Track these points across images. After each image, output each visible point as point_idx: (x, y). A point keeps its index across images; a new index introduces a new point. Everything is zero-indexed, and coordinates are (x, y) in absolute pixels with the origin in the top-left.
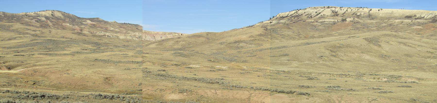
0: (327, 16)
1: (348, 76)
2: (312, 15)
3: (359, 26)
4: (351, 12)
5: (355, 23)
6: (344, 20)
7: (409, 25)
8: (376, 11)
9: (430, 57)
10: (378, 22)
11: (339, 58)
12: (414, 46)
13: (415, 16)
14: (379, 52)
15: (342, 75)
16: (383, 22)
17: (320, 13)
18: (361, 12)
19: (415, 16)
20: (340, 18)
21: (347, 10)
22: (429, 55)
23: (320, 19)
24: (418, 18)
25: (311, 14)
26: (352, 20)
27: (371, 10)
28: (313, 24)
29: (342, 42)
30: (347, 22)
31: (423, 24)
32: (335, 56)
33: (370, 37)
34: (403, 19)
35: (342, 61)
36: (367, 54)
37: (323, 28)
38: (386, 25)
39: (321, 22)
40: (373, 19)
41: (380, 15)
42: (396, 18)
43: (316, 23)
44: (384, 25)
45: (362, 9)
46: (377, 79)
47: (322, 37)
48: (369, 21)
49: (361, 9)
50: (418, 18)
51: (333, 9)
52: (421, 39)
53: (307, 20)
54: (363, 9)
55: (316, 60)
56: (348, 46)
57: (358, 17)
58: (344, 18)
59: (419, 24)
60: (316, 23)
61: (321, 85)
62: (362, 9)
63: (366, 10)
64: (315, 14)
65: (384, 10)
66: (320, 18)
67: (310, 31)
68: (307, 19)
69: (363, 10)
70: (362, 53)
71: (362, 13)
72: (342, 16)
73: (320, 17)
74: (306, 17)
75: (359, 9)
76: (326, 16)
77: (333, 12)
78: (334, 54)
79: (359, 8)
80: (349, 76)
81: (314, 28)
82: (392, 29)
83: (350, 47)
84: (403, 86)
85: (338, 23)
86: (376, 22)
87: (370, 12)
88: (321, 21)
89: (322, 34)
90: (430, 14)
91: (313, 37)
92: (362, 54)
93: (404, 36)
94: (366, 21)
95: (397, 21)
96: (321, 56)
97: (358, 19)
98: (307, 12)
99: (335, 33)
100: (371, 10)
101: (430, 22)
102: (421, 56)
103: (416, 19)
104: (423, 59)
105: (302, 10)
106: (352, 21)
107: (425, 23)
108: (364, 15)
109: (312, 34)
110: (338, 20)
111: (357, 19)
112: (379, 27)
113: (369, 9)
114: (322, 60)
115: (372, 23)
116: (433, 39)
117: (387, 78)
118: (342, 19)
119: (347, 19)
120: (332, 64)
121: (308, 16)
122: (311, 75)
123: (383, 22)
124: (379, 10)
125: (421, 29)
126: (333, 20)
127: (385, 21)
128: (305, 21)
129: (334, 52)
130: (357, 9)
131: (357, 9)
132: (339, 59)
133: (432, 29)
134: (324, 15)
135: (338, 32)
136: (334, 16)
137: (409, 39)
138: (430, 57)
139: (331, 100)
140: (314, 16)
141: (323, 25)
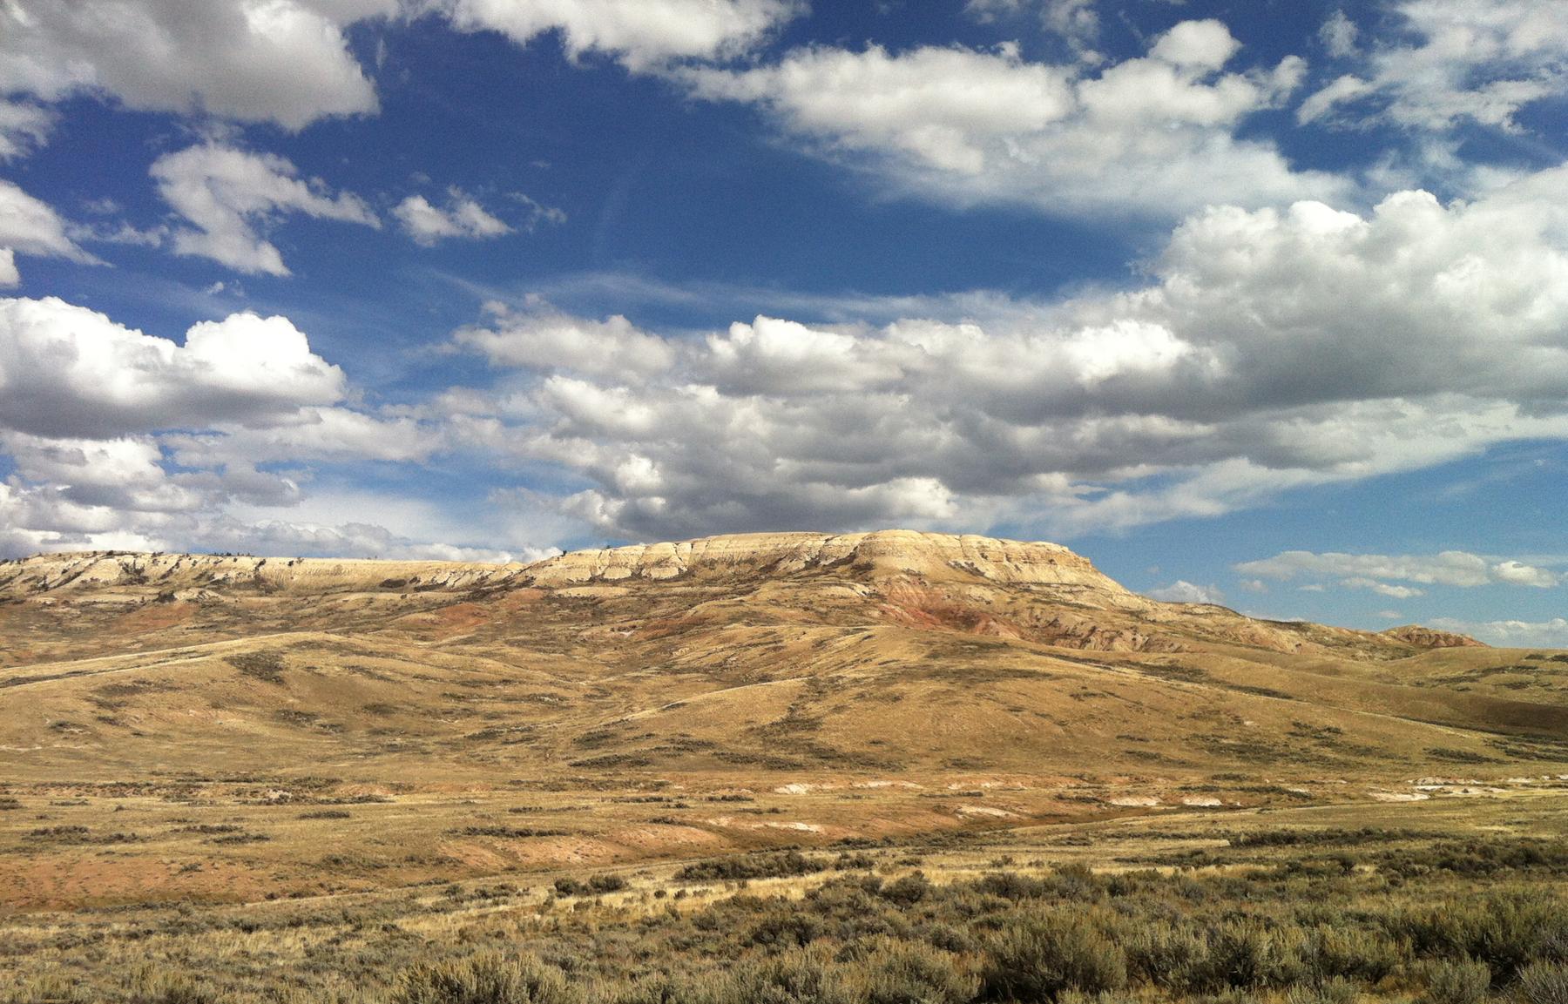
0: (106, 583)
1: (144, 790)
2: (48, 581)
3: (217, 617)
4: (191, 570)
5: (204, 606)
6: (165, 596)
7: (396, 610)
8: (283, 567)
9: (451, 713)
10: (287, 602)
11: (125, 726)
12: (399, 678)
13: (415, 580)
14: (277, 702)
15: (123, 788)
16: (306, 602)
17: (78, 574)
18: (229, 568)
19: (415, 580)
20: (150, 592)
21: (177, 564)
22: (450, 704)
23: (79, 595)
24: (424, 588)
25: (45, 578)
26: (195, 596)
27: (262, 563)
28: (51, 610)
29: (142, 672)
30: (176, 605)
31: (440, 605)
32: (111, 722)
33: (248, 651)
34: (373, 590)
35: (139, 739)
36: (230, 710)
37: (89, 625)
38: (315, 610)
39: (82, 605)
40: (269, 592)
41: (296, 578)
42: (351, 588)
43: (60, 610)
44: (308, 611)
45: (233, 558)
46: (248, 794)
47: (76, 655)
48: (255, 599)
49: (228, 561)
50: (424, 588)
51: (129, 560)
52: (426, 655)
53: (29, 599)
54: (235, 560)
55: (37, 740)
56: (165, 686)
57: (219, 585)
58: (166, 590)
59: (428, 607)
60: (61, 610)
61: (20, 829)
62: (233, 558)
63: (247, 563)
64: (62, 579)
65: (307, 561)
66: (79, 591)
67: (37, 638)
68: (28, 596)
69: (234, 564)
70: (216, 706)
71: (233, 574)
72: (161, 582)
73: (77, 588)
74: (27, 586)
75: (220, 559)
76: (100, 585)
77: (127, 571)
78: (110, 714)
79: (222, 555)
80: (147, 788)
81: (55, 625)
82: (336, 623)
83: (171, 689)
84: (317, 816)
85: (145, 608)
86: (281, 603)
87: (261, 568)
88: (81, 600)
89: (83, 646)
90: (466, 572)
91: (45, 658)
92: (213, 712)
93: (371, 647)
94: (244, 599)
95: (353, 597)
96: (61, 725)
97: (216, 595)
98: (31, 570)
99: (129, 641)
100: (262, 563)
101: (463, 599)
102: (421, 711)
103: (417, 590)
104: (430, 719)
105: (12, 562)
106: (196, 601)
107: (449, 604)
108: (239, 581)
109: (40, 647)
110: (146, 599)
111: (212, 594)
112: (288, 619)
113: (258, 560)
114: (62, 736)
115: (265, 607)
116: (471, 655)
117: (1410, 764)
118: (159, 594)
119: (176, 596)
120: (97, 750)
121: (32, 583)
122: (7, 793)
123: (306, 602)
124: (291, 564)
125: (432, 622)
126: (125, 599)
127: (310, 599)
128: (22, 602)
129: (110, 706)
130: (213, 560)
131: (213, 560)
132: (126, 732)
133: (472, 620)
134: (92, 579)
135: (141, 637)
136: (130, 582)
137: (386, 655)
138: (451, 713)
139: (28, 881)
140: (56, 584)
141: (89, 616)
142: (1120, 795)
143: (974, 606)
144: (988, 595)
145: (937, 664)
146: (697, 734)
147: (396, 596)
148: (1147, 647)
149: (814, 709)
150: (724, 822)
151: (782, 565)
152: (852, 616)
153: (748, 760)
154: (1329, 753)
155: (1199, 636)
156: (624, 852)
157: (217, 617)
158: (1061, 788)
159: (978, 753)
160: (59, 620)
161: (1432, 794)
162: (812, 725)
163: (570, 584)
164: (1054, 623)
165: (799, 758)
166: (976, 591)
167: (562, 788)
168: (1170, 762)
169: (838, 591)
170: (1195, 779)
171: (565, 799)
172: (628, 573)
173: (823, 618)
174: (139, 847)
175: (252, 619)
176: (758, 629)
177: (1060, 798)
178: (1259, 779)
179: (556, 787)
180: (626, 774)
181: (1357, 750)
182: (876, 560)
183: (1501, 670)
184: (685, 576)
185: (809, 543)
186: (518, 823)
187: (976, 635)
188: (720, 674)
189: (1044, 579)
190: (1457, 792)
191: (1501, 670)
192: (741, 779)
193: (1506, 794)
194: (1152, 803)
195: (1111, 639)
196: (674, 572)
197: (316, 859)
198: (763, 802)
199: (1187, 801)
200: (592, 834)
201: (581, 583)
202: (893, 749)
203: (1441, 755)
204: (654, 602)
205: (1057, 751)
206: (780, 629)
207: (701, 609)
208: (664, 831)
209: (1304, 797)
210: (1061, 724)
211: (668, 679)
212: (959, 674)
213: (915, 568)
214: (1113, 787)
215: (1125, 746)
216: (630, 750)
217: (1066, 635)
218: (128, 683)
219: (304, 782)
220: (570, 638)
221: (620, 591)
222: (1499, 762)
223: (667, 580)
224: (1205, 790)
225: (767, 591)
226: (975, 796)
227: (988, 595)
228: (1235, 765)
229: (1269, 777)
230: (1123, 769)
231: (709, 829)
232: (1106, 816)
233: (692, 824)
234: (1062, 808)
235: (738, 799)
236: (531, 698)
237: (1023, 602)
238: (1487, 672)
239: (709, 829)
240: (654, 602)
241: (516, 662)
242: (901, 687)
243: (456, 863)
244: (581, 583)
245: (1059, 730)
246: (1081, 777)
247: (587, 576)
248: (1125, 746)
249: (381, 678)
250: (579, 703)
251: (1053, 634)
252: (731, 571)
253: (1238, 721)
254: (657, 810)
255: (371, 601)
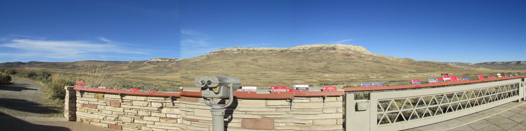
7: (271, 54)
13: (273, 50)
19: (273, 50)
20: (241, 52)
22: (279, 65)
32: (238, 66)
40: (255, 52)
42: (265, 51)
47: (233, 59)
49: (250, 48)
51: (238, 48)
56: (244, 62)
57: (249, 51)
58: (243, 52)
60: (230, 54)
63: (252, 48)
78: (238, 65)
81: (229, 55)
88: (232, 53)
91: (229, 59)
95: (265, 52)
115: (255, 53)
129: (238, 65)
133: (281, 55)
142: (371, 76)
143: (350, 54)
144: (352, 52)
145: (345, 61)
146: (313, 68)
147: (271, 52)
148: (373, 59)
149: (329, 66)
150: (319, 79)
151: (323, 48)
152: (333, 55)
153: (320, 72)
154: (397, 72)
155: (380, 58)
156: (306, 82)
157: (249, 54)
158: (363, 76)
159: (351, 71)
160: (230, 55)
161: (409, 76)
162: (328, 68)
163: (296, 50)
164: (360, 56)
165: (327, 72)
166: (350, 52)
167: (295, 74)
168: (377, 73)
169: (331, 51)
170: (380, 75)
171: (296, 76)
172: (302, 49)
173: (329, 55)
174: (246, 80)
175: (253, 55)
176: (320, 56)
177: (363, 77)
178: (388, 75)
179: (295, 74)
180: (303, 73)
181: (400, 71)
182: (336, 48)
183: (417, 63)
184: (309, 49)
185: (327, 45)
186: (292, 79)
187: (350, 57)
188: (315, 61)
189: (359, 51)
190: (412, 76)
191: (417, 63)
192: (319, 74)
193: (418, 76)
194: (375, 77)
195: (368, 58)
196: (308, 49)
197: (268, 82)
198: (323, 77)
199: (380, 77)
200: (301, 80)
201: (297, 50)
202: (340, 71)
203: (410, 72)
204: (305, 52)
205: (362, 72)
206: (323, 56)
207: (312, 53)
208: (311, 80)
209: (394, 77)
210: (362, 68)
211: (308, 62)
212: (348, 62)
213: (341, 49)
214: (370, 75)
215: (371, 71)
216: (303, 70)
217: (362, 57)
218: (240, 62)
219: (263, 74)
220: (296, 57)
221: (302, 51)
222: (417, 73)
223: (307, 50)
224: (382, 76)
225: (321, 51)
226: (352, 76)
227: (352, 52)
228: (385, 73)
229: (389, 74)
230: (371, 73)
231: (317, 80)
232: (369, 79)
233: (314, 79)
234: (363, 78)
235: (319, 76)
236: (290, 64)
237: (356, 53)
238: (415, 63)
239: (317, 80)
240: (305, 52)
241: (287, 60)
242: (340, 63)
243: (285, 83)
244: (297, 50)
245: (362, 69)
246: (365, 74)
247: (298, 49)
248: (371, 71)
249: (270, 62)
250: (297, 64)
251: (360, 57)
252: (316, 49)
253: (385, 68)
254: (308, 77)
255: (268, 53)
